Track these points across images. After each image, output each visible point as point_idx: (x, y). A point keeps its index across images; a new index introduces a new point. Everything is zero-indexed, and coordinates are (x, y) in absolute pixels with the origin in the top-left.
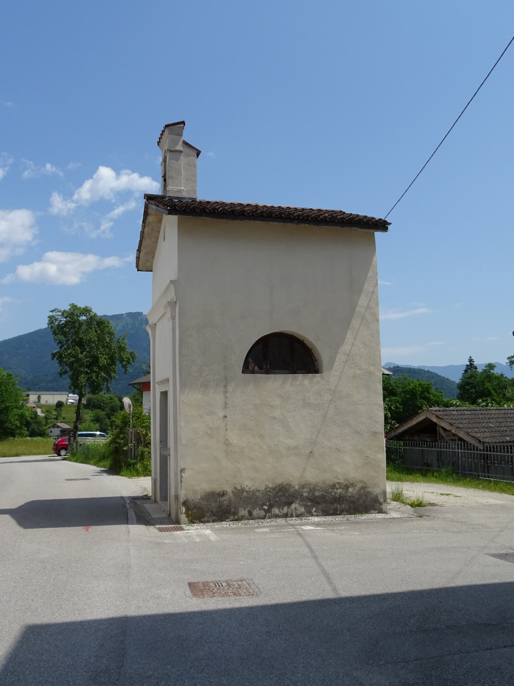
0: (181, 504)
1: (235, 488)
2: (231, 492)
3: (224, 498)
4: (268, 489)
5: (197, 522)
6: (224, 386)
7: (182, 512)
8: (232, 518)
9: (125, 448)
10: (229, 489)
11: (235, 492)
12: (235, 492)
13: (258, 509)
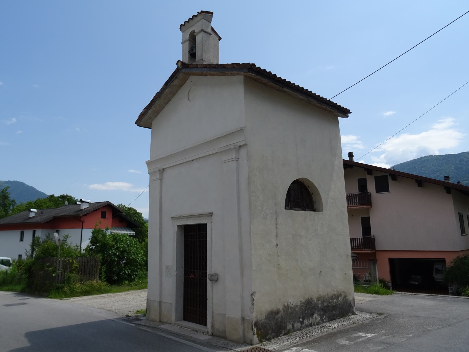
0: (253, 325)
1: (284, 306)
2: (282, 309)
3: (278, 315)
4: (302, 304)
5: (264, 341)
6: (276, 219)
7: (254, 332)
8: (283, 333)
9: (53, 275)
10: (281, 308)
11: (284, 309)
12: (284, 309)
13: (297, 322)
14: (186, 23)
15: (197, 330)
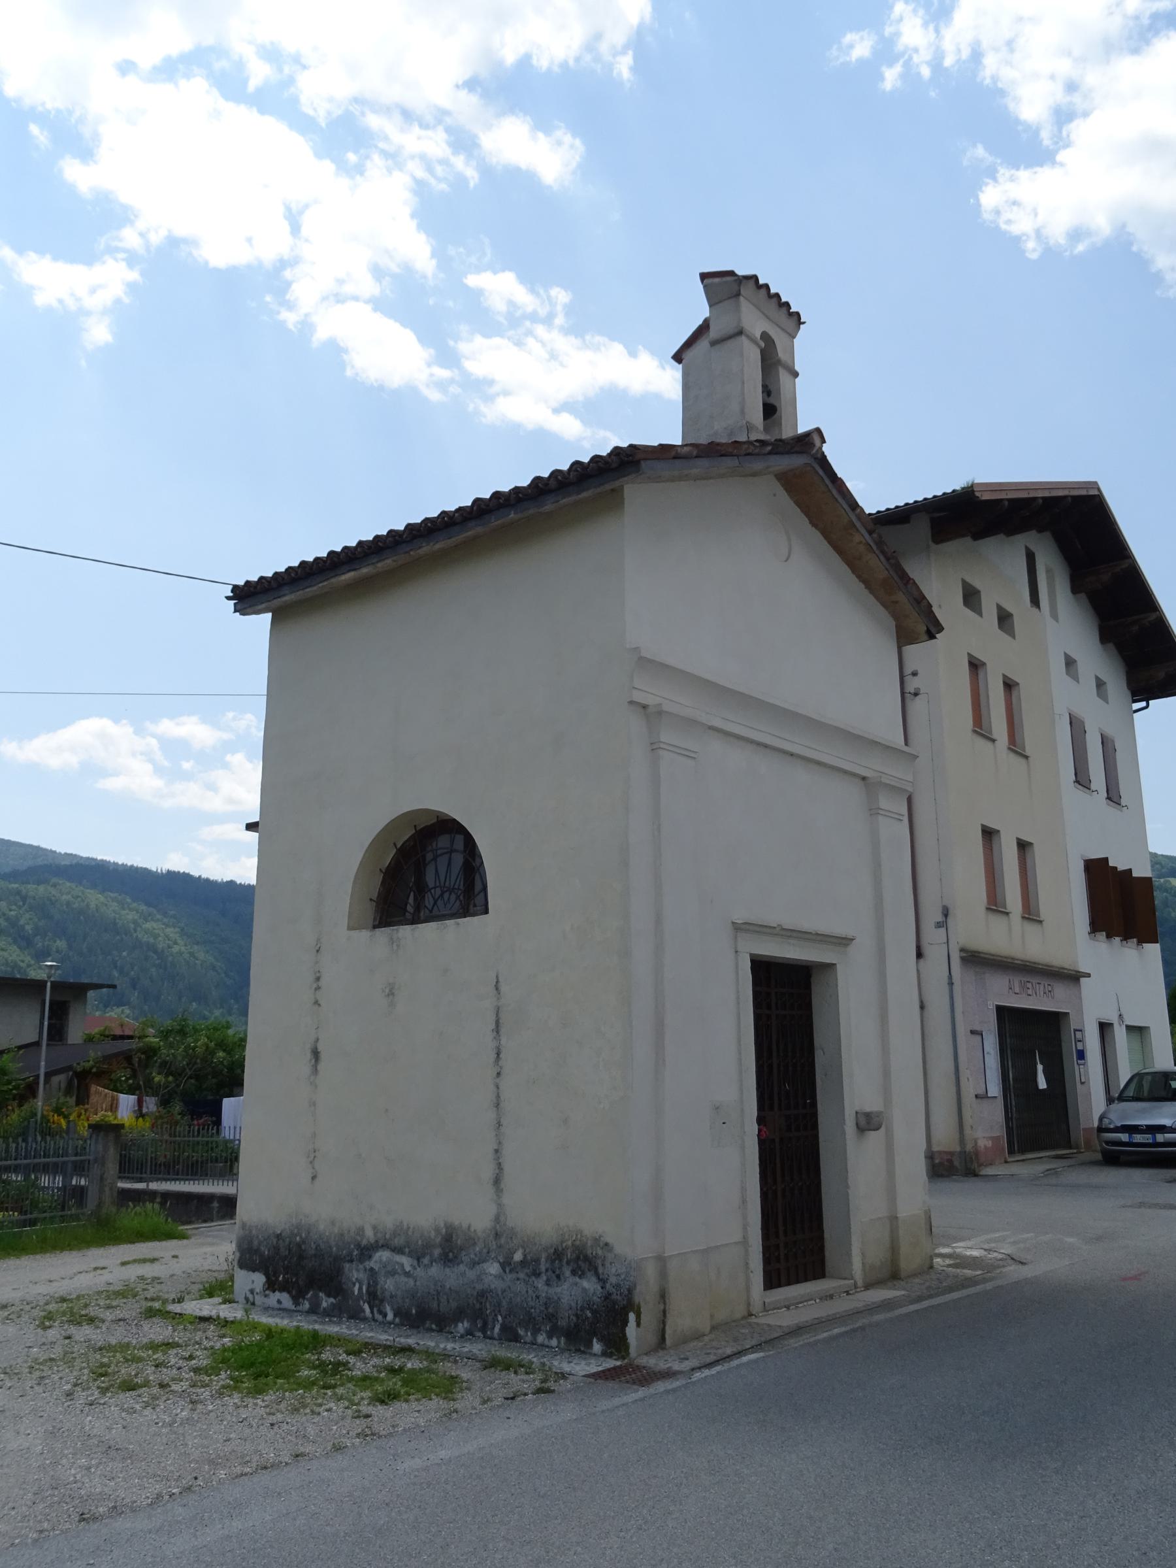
14: (775, 300)
15: (831, 1292)
